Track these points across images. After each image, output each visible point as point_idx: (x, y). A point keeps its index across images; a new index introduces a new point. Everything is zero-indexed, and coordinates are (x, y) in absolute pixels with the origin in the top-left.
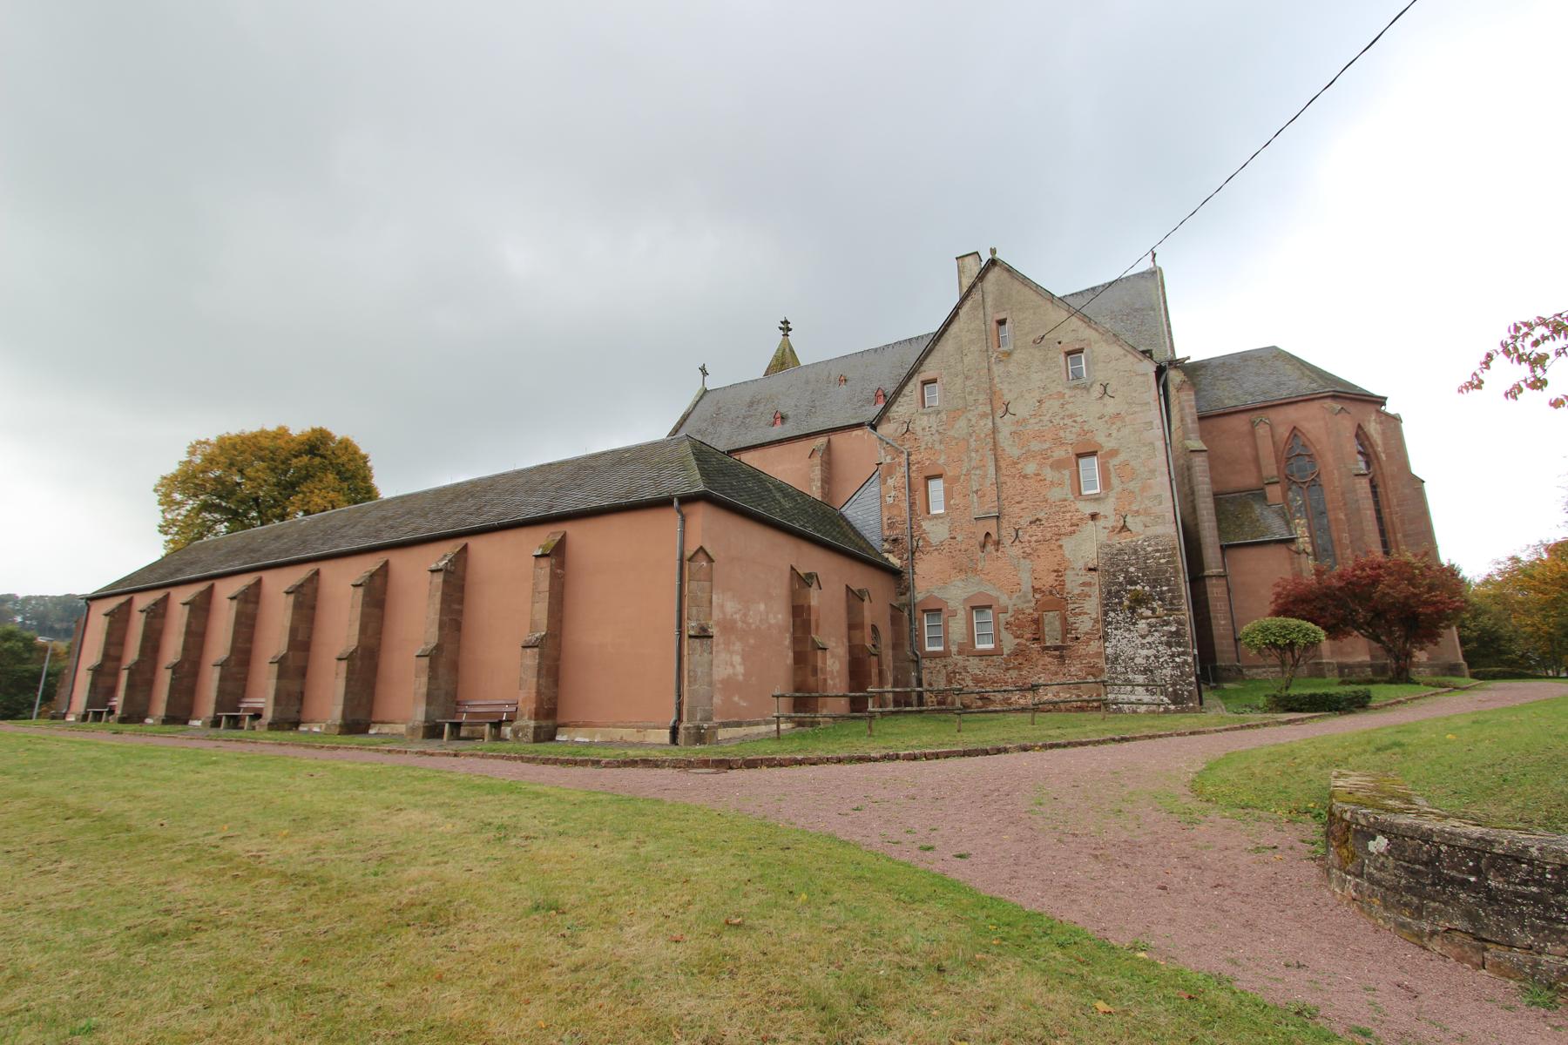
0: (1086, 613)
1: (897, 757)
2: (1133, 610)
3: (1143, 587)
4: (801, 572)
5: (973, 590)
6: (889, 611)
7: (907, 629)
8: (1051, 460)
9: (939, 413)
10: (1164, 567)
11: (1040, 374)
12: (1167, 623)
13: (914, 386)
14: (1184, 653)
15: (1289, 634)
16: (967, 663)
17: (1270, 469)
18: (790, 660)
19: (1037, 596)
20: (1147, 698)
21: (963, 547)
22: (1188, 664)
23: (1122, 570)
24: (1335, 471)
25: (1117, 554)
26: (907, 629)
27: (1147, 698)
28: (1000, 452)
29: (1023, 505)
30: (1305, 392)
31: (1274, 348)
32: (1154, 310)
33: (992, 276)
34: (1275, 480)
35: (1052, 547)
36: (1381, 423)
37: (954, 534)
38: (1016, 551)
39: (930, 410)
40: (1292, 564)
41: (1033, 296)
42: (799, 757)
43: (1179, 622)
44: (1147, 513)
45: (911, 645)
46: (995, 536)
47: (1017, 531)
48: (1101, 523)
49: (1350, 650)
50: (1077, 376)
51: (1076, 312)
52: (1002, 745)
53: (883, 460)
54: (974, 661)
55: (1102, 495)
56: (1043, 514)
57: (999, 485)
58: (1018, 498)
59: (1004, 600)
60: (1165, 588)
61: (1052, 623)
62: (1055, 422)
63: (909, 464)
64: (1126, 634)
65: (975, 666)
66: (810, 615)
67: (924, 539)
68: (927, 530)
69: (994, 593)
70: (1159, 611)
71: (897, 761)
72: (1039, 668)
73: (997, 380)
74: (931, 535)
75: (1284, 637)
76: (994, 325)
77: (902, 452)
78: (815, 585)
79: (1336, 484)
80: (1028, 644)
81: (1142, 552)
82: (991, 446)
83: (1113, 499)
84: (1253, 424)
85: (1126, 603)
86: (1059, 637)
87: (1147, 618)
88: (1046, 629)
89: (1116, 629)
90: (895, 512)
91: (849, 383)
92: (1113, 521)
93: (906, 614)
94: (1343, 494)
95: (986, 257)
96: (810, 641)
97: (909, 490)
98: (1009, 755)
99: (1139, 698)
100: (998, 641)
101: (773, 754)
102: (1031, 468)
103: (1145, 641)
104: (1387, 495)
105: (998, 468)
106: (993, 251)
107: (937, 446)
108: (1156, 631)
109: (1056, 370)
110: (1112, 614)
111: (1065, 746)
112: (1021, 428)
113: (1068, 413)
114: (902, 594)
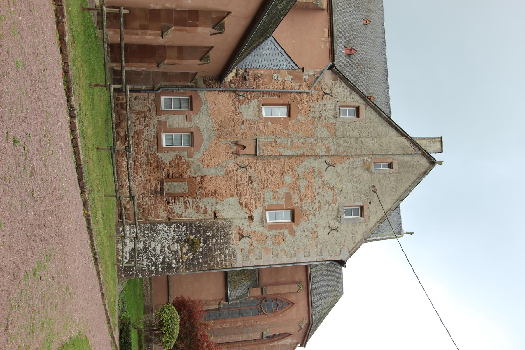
0: (186, 210)
1: (72, 117)
2: (187, 241)
3: (202, 248)
4: (225, 20)
5: (205, 134)
6: (192, 71)
7: (178, 84)
8: (292, 193)
9: (335, 117)
10: (214, 260)
11: (351, 189)
12: (177, 262)
13: (357, 101)
14: (157, 271)
15: (169, 333)
16: (152, 127)
17: (270, 291)
18: (152, 6)
19: (199, 178)
20: (127, 249)
21: (237, 129)
22: (150, 274)
23: (214, 234)
24: (265, 323)
25: (224, 231)
26: (178, 84)
27: (127, 249)
28: (301, 159)
29: (263, 173)
30: (314, 310)
31: (342, 294)
32: (377, 233)
33: (424, 162)
34: (264, 293)
35: (233, 190)
36: (291, 344)
37: (246, 123)
38: (231, 166)
39: (338, 111)
40: (213, 300)
41: (404, 188)
42: (67, 39)
43: (178, 269)
44: (250, 251)
45: (166, 86)
46: (242, 152)
47: (245, 167)
48: (246, 222)
50: (347, 212)
51: (386, 217)
52: (88, 188)
53: (305, 73)
54: (153, 132)
55: (265, 224)
56: (255, 185)
57: (278, 157)
58: (268, 169)
59: (197, 156)
60: (200, 260)
61: (181, 187)
62: (317, 197)
63: (300, 93)
64: (171, 237)
65: (150, 132)
66: (190, 26)
67: (244, 101)
68: (251, 104)
69: (202, 149)
70: (186, 257)
71: (69, 118)
72: (148, 177)
73: (352, 160)
74: (247, 106)
75: (167, 330)
76: (390, 160)
77: (310, 88)
78: (214, 31)
79: (258, 323)
80: (165, 170)
81: (225, 247)
82: (307, 153)
83: (261, 231)
84: (298, 283)
85: (192, 237)
86: (170, 192)
87: (181, 250)
88: (175, 183)
89: (174, 231)
90: (266, 80)
91: (364, 26)
92: (247, 229)
93: (189, 84)
94: (252, 326)
95: (437, 157)
96: (169, 25)
97: (282, 92)
98: (80, 195)
99: (128, 244)
100: (168, 150)
101: (69, 13)
102: (288, 179)
103: (166, 248)
104: (250, 345)
105: (290, 157)
106: (440, 163)
107: (311, 115)
108: (173, 255)
109: (352, 199)
110: (184, 228)
111: (89, 228)
112: (316, 174)
113: (322, 206)
114: (204, 81)
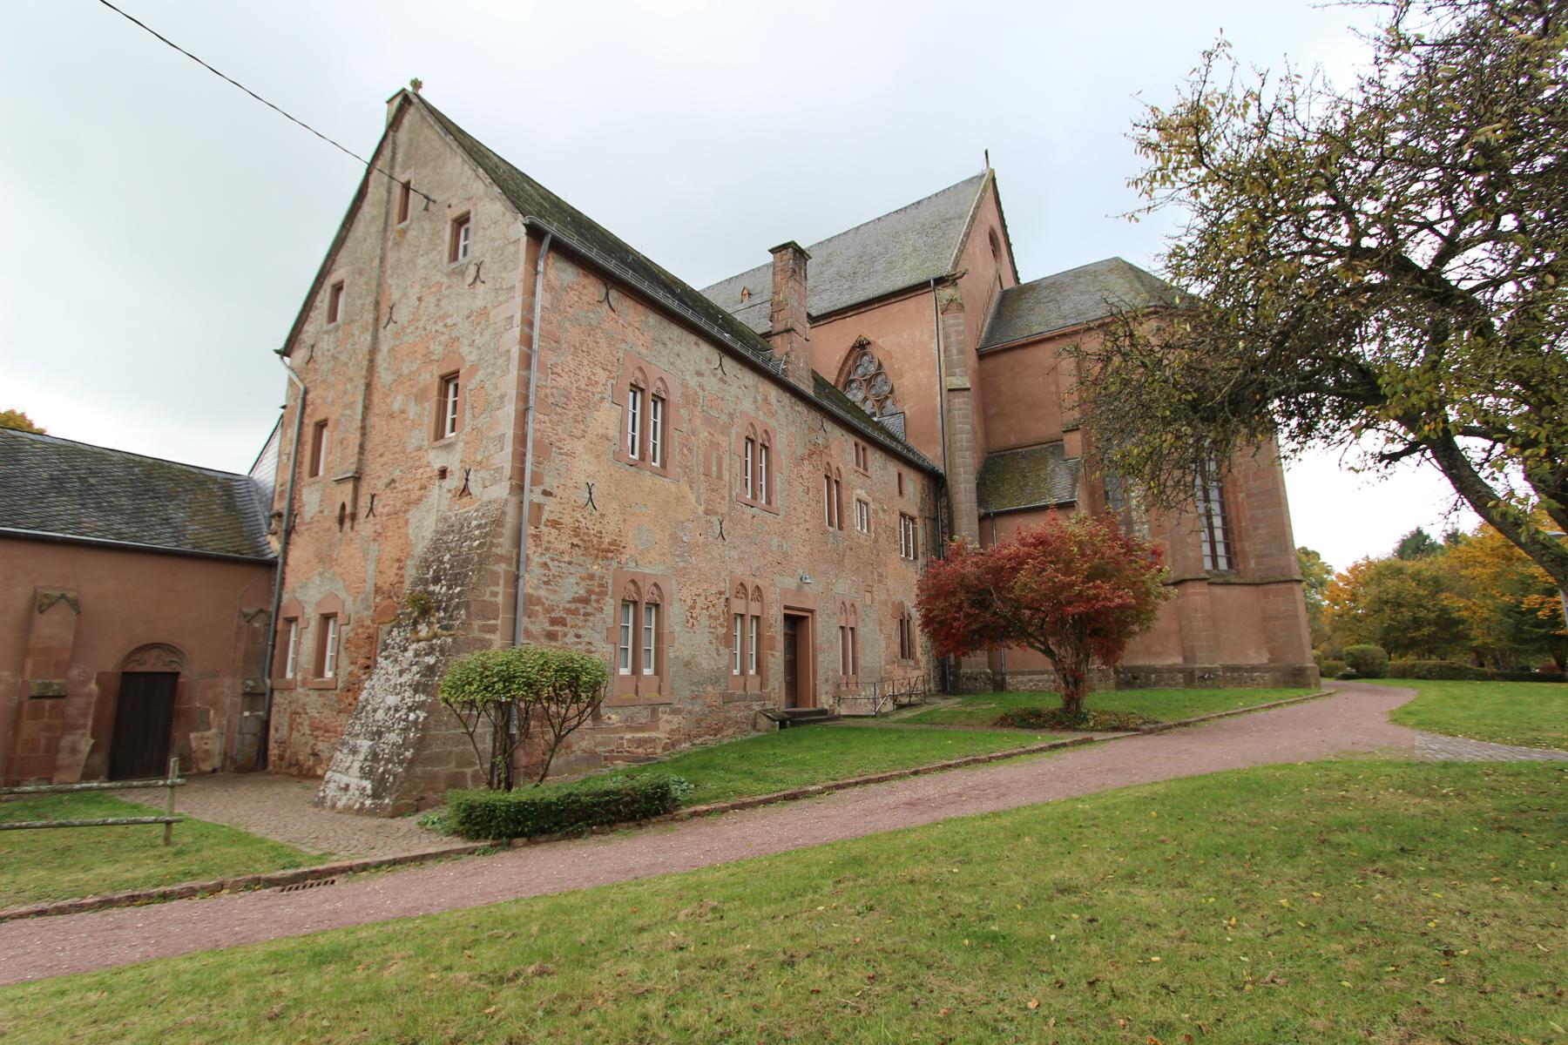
49: (1159, 648)
